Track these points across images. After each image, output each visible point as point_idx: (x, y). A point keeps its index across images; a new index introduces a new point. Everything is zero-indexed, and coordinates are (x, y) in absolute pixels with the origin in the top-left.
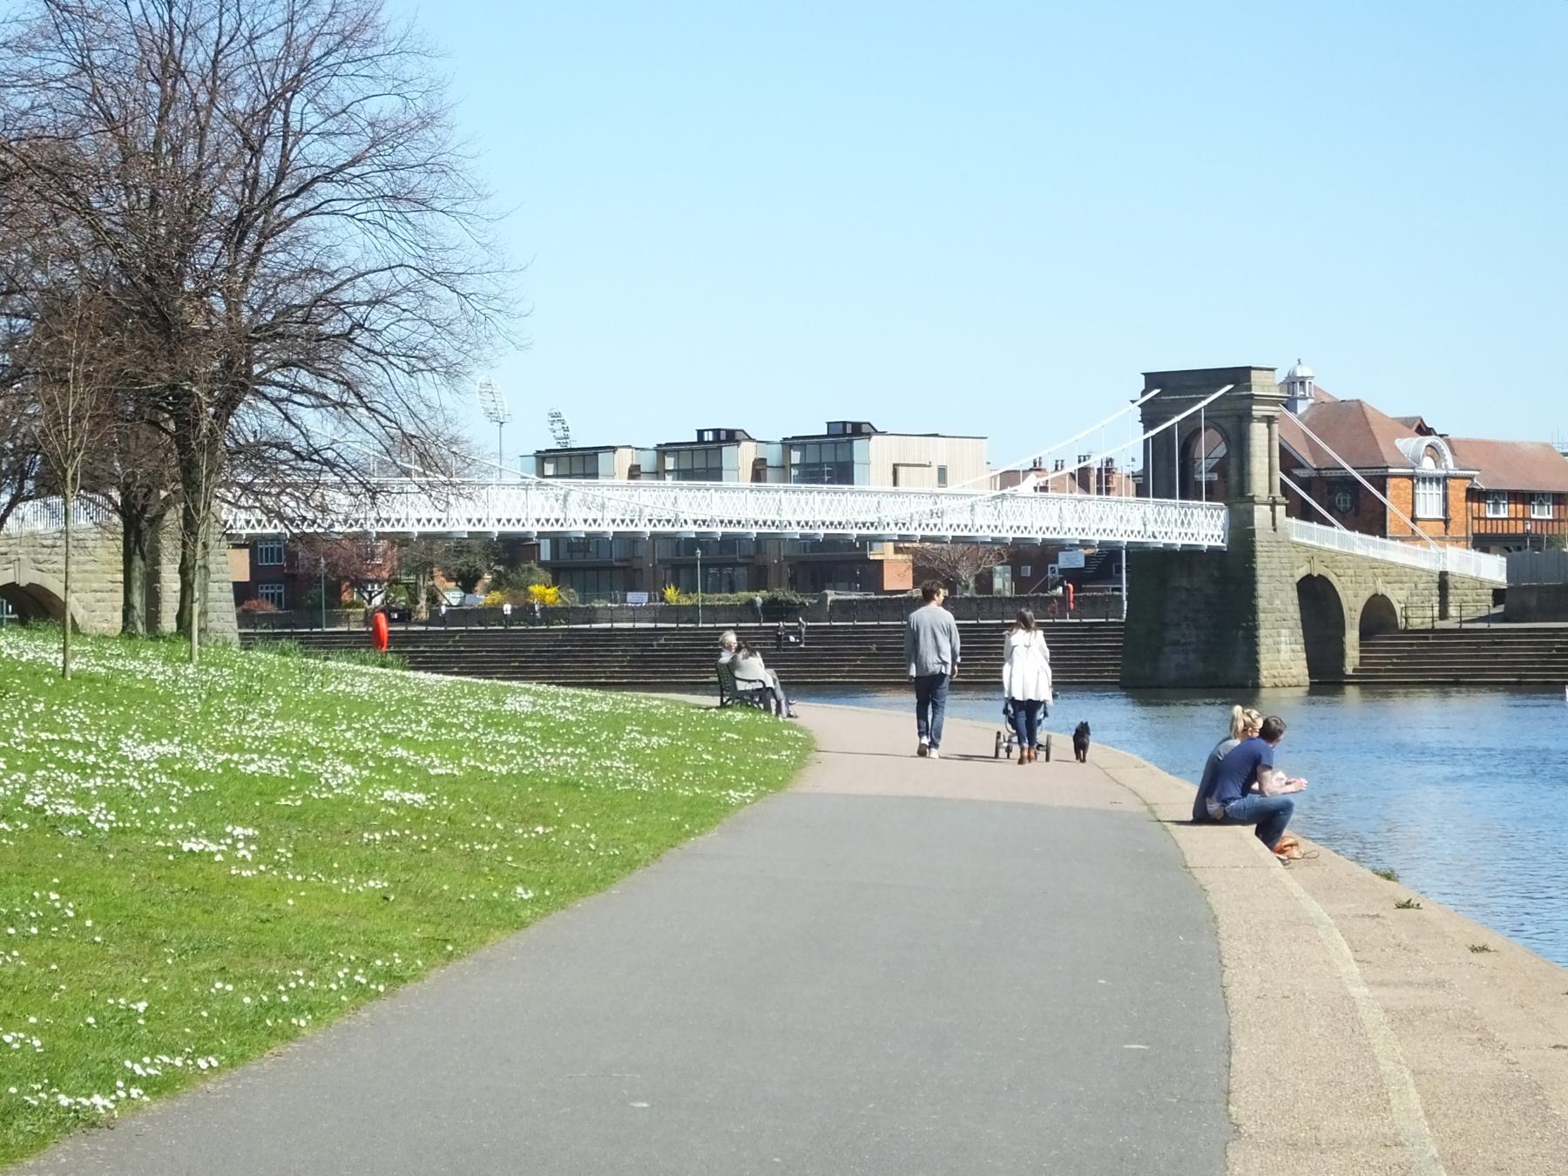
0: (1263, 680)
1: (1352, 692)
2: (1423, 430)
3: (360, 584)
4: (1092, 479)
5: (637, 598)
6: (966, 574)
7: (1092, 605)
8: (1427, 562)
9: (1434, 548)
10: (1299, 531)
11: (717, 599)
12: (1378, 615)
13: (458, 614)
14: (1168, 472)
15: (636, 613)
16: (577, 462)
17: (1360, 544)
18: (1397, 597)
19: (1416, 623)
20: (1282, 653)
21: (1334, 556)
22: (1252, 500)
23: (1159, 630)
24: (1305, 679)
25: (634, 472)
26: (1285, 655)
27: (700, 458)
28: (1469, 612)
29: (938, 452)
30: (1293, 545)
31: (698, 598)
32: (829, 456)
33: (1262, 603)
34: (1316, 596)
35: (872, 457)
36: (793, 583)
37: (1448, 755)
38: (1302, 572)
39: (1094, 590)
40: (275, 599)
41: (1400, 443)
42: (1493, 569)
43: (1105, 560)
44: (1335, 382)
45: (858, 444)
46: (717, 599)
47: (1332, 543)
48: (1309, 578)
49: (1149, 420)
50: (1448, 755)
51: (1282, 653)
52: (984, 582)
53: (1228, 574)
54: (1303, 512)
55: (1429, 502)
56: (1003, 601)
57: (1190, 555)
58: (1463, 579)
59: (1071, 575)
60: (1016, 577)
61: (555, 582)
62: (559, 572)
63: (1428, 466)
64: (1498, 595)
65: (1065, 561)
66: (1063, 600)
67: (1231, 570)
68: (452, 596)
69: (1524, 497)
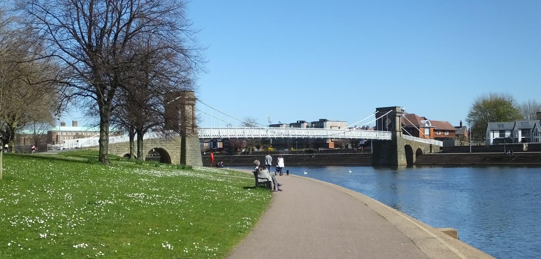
0: (399, 163)
1: (414, 166)
2: (425, 119)
3: (240, 148)
4: (366, 128)
5: (287, 150)
6: (343, 145)
7: (365, 151)
8: (426, 142)
9: (429, 140)
10: (404, 136)
11: (300, 150)
12: (419, 152)
13: (257, 153)
14: (380, 126)
15: (286, 152)
16: (298, 125)
17: (415, 139)
18: (423, 149)
19: (426, 153)
20: (402, 159)
21: (411, 142)
22: (396, 131)
23: (376, 156)
24: (406, 164)
25: (307, 127)
26: (402, 159)
27: (298, 125)
28: (436, 151)
29: (339, 124)
30: (405, 139)
31: (297, 150)
32: (320, 124)
33: (398, 150)
34: (408, 149)
35: (328, 124)
36: (313, 147)
37: (430, 182)
38: (405, 144)
39: (366, 148)
40: (226, 150)
41: (421, 121)
42: (441, 144)
43: (369, 142)
44: (409, 111)
45: (324, 123)
46: (300, 150)
47: (410, 138)
48: (406, 145)
49: (377, 117)
50: (430, 182)
51: (402, 159)
52: (347, 146)
53: (392, 144)
54: (404, 133)
55: (427, 132)
56: (350, 150)
57: (385, 141)
58: (434, 145)
59: (362, 145)
60: (352, 146)
61: (273, 147)
62: (274, 146)
63: (427, 125)
64: (441, 148)
65: (361, 143)
66: (361, 150)
67: (392, 144)
68: (256, 150)
69: (444, 131)
